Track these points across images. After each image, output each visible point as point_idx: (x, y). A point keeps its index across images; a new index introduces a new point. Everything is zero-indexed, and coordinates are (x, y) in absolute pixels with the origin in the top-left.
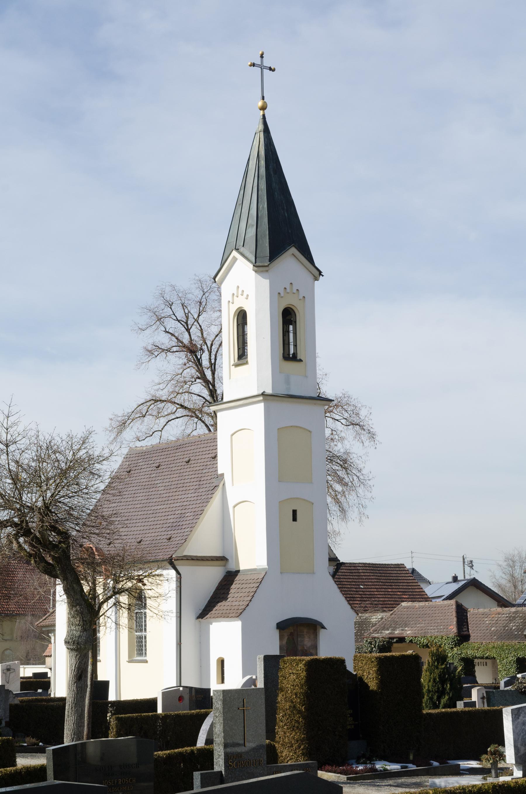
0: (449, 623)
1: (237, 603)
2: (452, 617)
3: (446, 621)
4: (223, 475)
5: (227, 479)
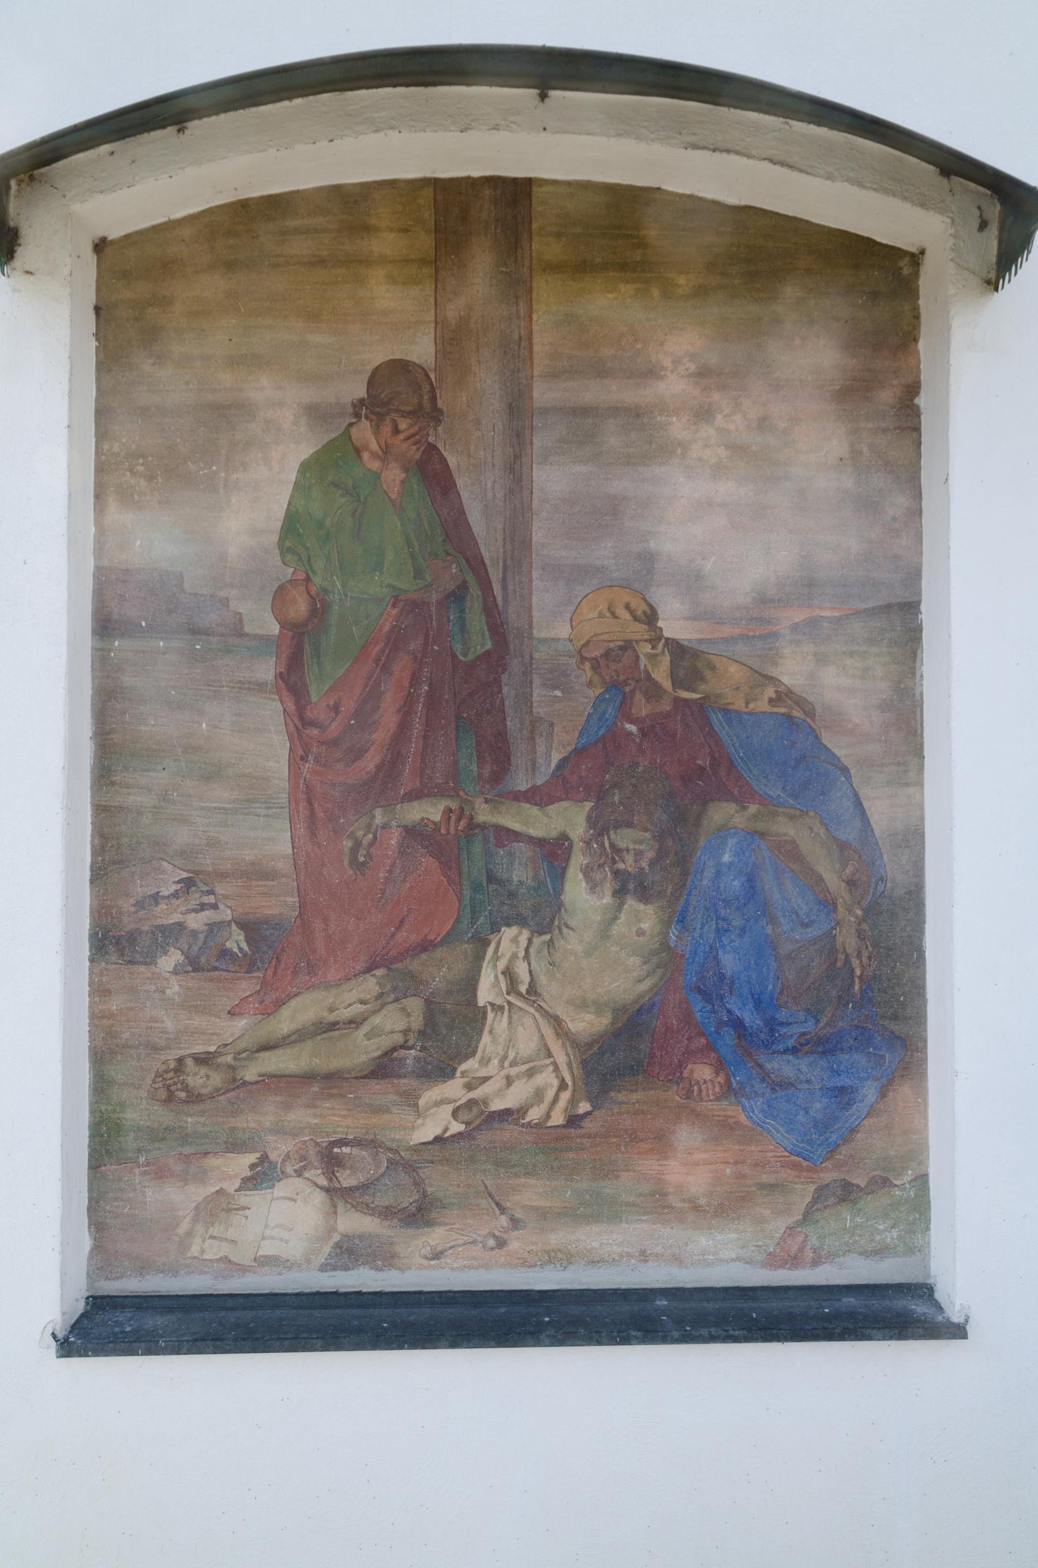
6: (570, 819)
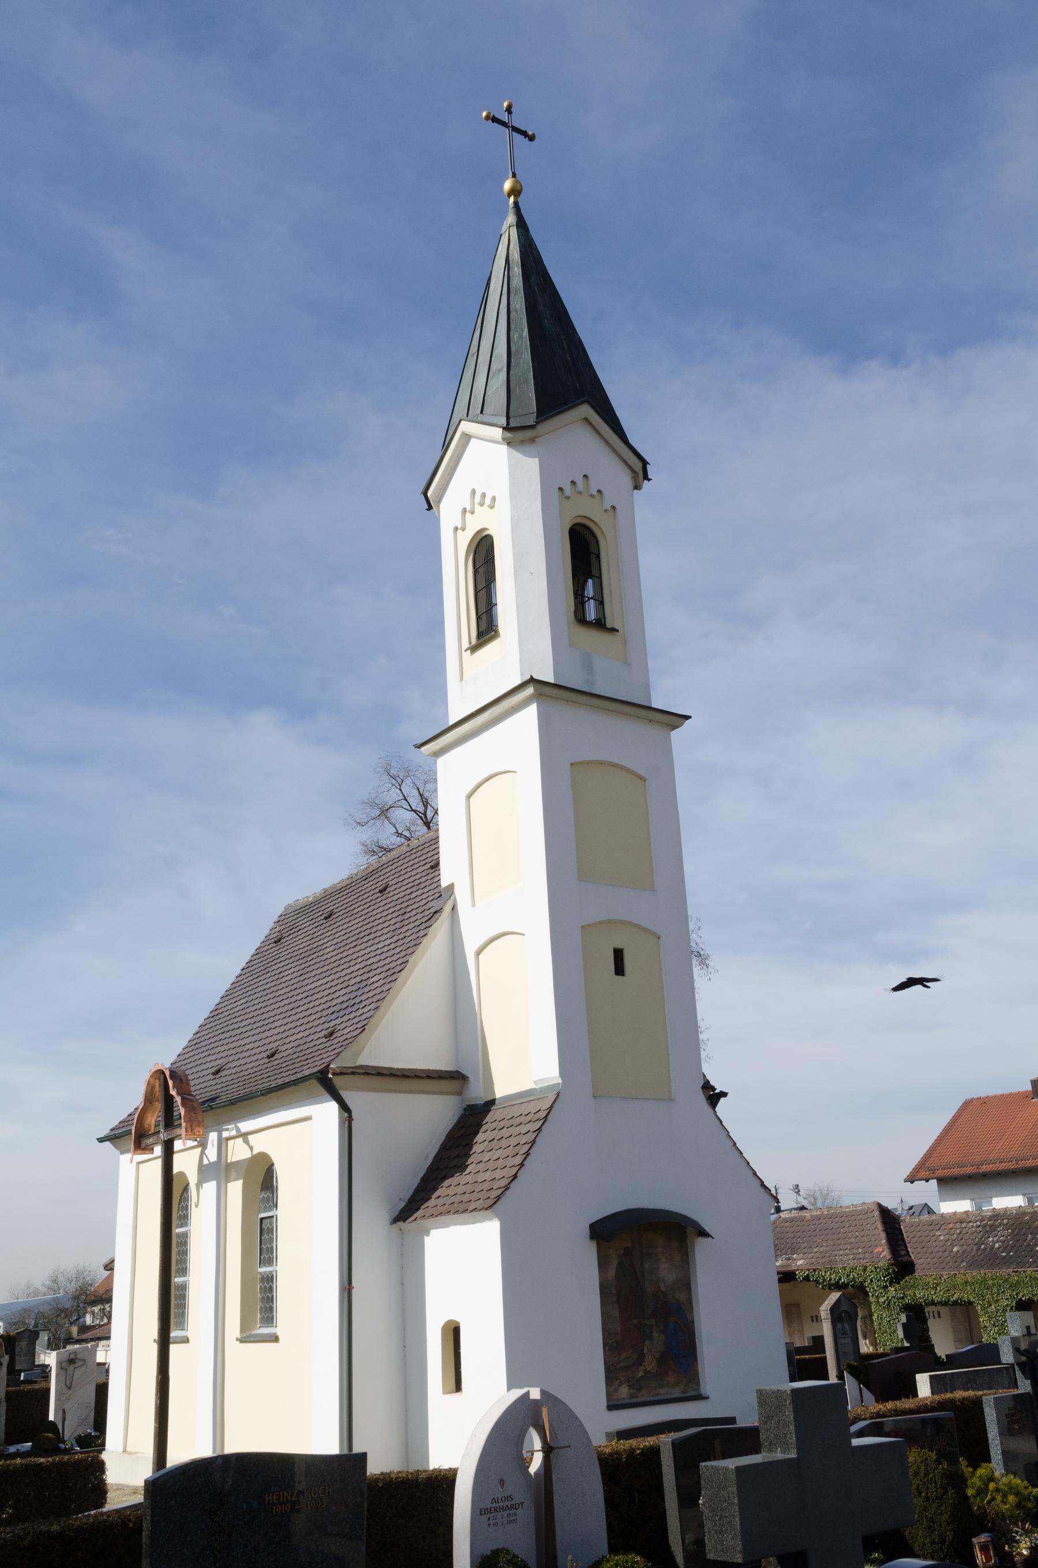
0: (873, 1243)
1: (488, 1176)
2: (876, 1232)
3: (865, 1239)
4: (451, 887)
5: (461, 895)
6: (652, 1322)
